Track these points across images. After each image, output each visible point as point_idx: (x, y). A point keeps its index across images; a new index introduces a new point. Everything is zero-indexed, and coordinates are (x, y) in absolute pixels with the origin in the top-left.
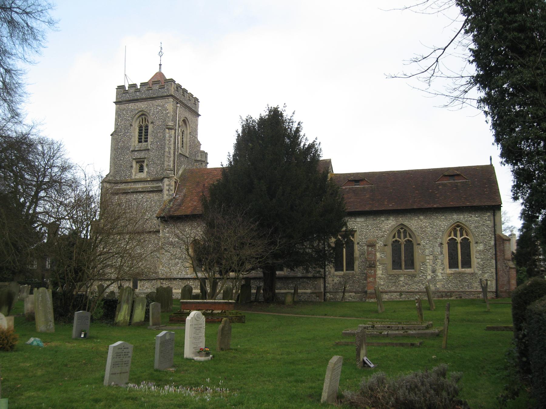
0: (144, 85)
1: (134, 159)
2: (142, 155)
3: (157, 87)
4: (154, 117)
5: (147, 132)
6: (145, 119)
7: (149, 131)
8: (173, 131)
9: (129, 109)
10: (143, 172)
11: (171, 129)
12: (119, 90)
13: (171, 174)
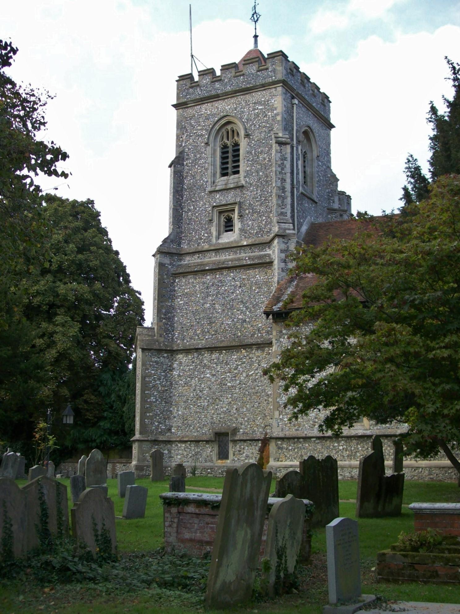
0: (227, 69)
1: (214, 207)
2: (230, 197)
3: (253, 69)
4: (251, 126)
5: (236, 156)
6: (233, 131)
7: (242, 152)
8: (288, 147)
9: (202, 114)
10: (232, 230)
11: (285, 144)
12: (181, 82)
13: (289, 229)
